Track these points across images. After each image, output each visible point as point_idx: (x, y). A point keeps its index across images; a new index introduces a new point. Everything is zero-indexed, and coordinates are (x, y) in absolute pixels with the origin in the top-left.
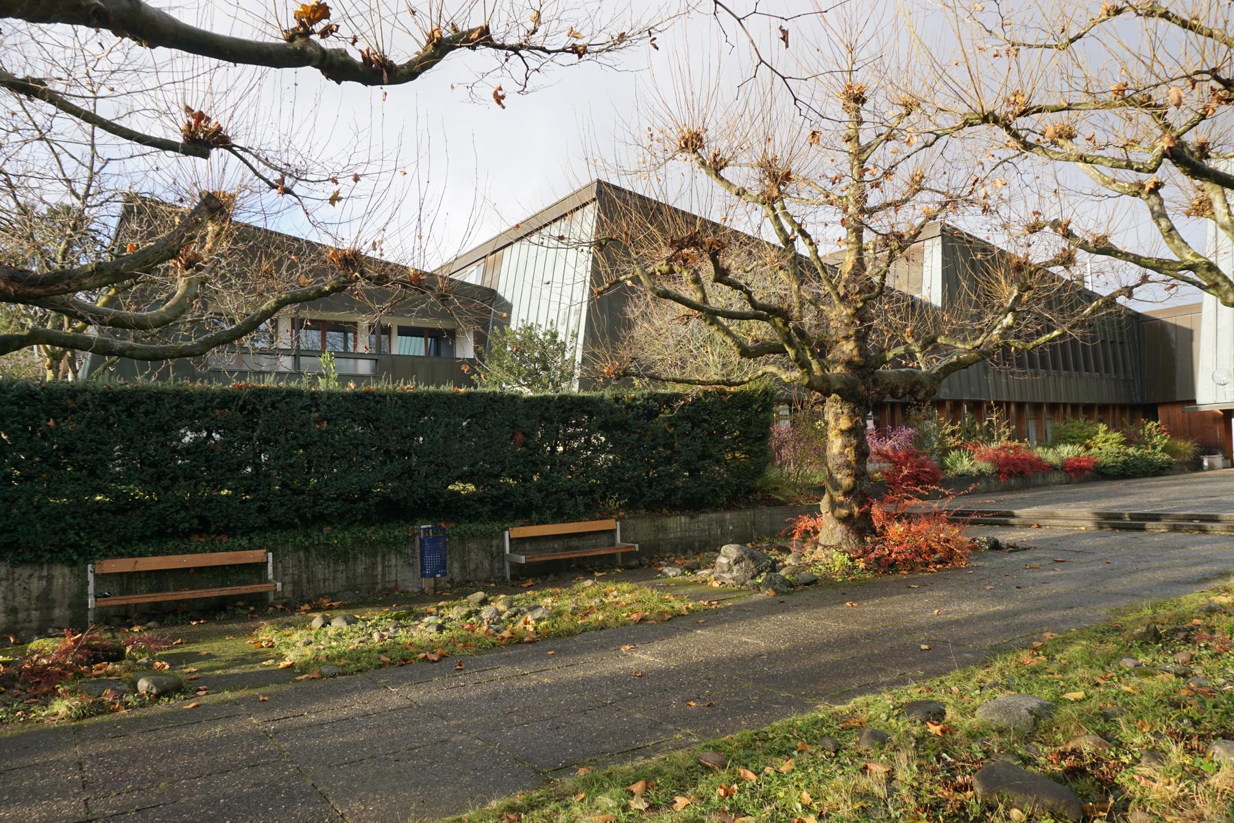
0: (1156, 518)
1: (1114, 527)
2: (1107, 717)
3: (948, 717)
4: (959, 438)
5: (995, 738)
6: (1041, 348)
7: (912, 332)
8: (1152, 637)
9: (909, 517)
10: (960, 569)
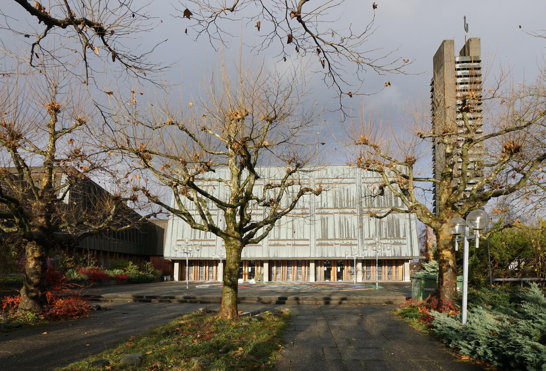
0: (155, 297)
1: (140, 301)
2: (162, 357)
3: (111, 364)
4: (73, 264)
5: (130, 367)
6: (122, 231)
7: (65, 216)
8: (167, 334)
9: (67, 297)
10: (86, 317)
